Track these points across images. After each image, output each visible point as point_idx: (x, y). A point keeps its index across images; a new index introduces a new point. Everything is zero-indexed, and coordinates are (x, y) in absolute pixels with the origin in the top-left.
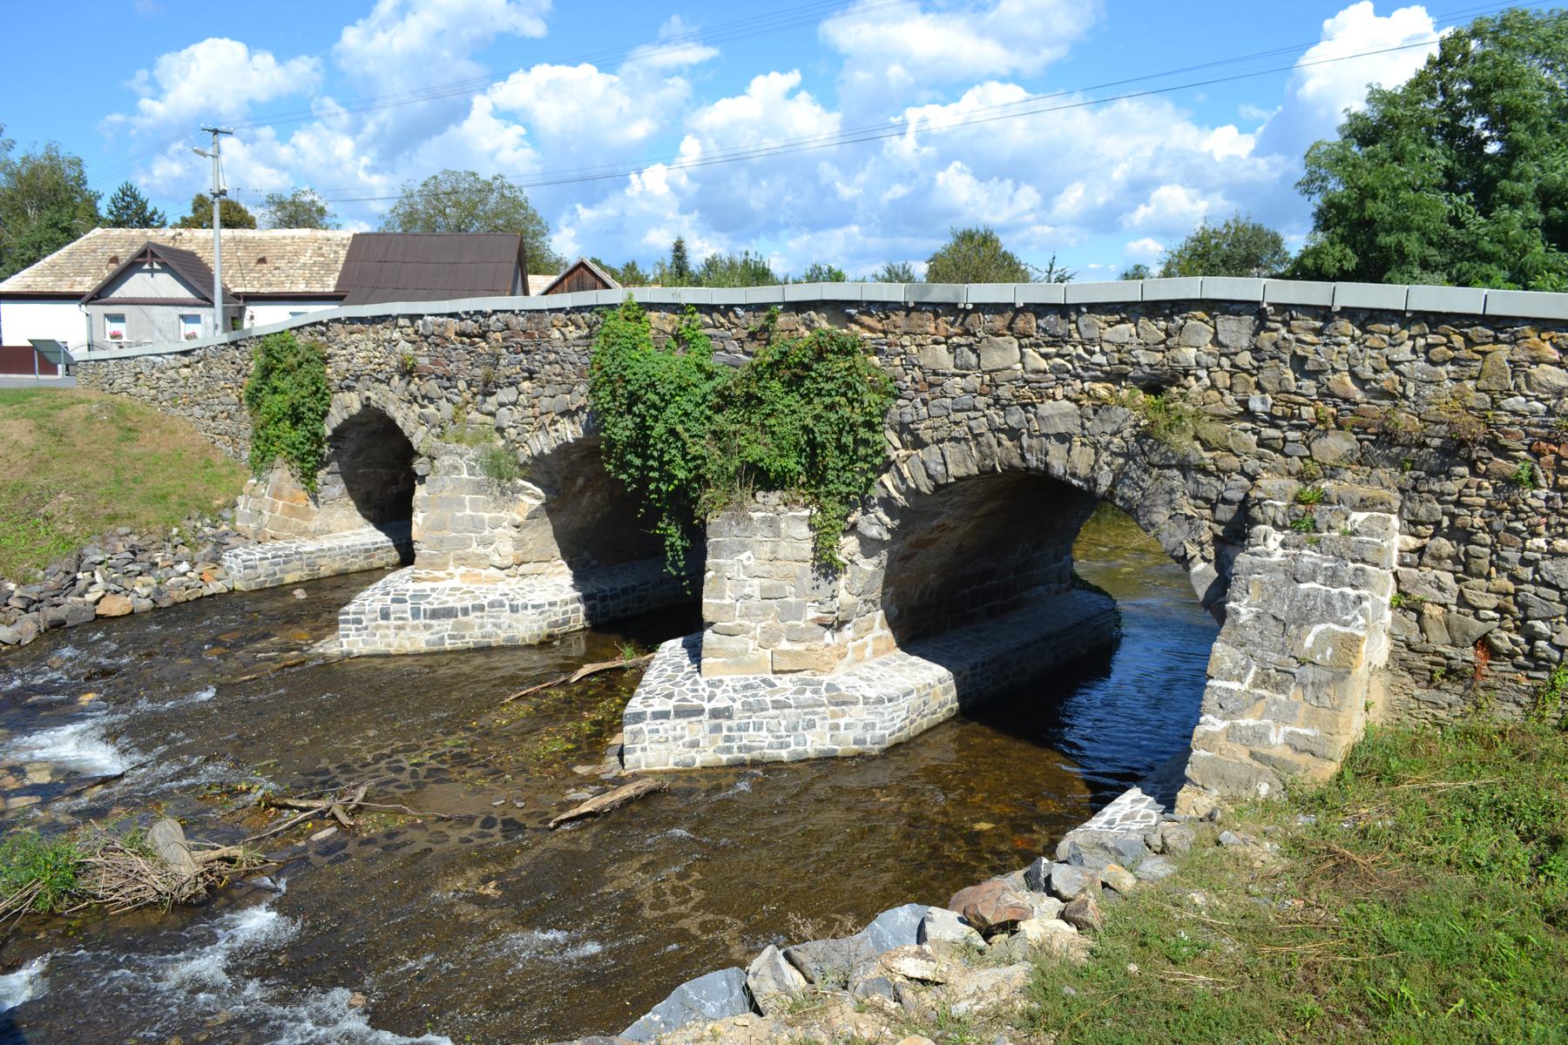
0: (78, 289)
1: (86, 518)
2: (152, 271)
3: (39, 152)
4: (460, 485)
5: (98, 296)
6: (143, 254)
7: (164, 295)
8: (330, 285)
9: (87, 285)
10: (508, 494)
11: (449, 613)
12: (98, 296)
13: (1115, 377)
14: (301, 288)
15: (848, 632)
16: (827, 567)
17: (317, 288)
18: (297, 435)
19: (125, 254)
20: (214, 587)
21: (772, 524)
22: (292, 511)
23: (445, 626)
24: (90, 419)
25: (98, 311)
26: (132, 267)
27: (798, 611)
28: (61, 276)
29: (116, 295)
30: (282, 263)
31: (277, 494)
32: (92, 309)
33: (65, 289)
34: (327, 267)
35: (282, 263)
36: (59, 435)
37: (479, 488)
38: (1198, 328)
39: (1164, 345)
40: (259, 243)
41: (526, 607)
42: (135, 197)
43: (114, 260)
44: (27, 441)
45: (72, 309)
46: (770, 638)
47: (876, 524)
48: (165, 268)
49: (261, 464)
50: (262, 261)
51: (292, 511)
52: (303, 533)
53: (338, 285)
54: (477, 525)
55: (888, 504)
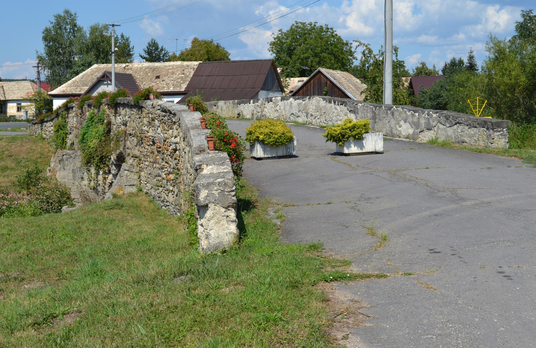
14: (171, 89)
17: (178, 90)
35: (166, 78)
50: (158, 77)
53: (186, 88)
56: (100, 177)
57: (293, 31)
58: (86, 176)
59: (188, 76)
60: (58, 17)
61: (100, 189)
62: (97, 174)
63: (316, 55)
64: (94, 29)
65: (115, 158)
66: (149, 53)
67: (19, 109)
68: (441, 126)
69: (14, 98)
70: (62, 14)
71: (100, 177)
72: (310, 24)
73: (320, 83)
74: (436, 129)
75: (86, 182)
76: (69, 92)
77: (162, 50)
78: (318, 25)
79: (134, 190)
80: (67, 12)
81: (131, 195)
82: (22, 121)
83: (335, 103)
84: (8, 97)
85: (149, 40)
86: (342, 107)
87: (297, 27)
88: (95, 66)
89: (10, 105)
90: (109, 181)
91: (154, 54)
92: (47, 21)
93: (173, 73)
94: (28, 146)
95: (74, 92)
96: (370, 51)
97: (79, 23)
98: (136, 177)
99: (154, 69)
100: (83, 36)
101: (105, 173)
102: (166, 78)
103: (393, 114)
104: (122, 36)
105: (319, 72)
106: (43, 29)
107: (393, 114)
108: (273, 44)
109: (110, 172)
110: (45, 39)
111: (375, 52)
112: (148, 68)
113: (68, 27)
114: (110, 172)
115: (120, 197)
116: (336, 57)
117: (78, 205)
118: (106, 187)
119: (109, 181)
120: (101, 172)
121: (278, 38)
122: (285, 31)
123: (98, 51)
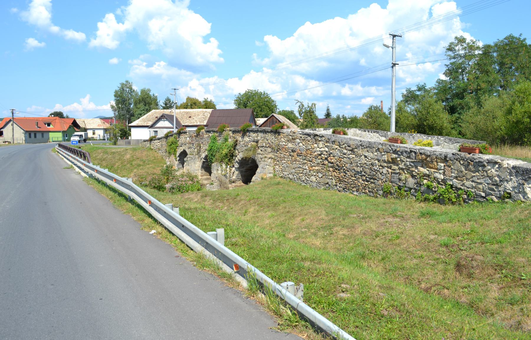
0: (148, 125)
2: (164, 121)
5: (152, 127)
6: (162, 116)
9: (150, 124)
12: (152, 127)
13: (254, 141)
19: (159, 116)
25: (152, 130)
26: (159, 120)
35: (194, 118)
39: (257, 137)
43: (157, 117)
45: (146, 130)
47: (237, 165)
48: (167, 120)
50: (190, 117)
55: (237, 161)
56: (228, 169)
57: (246, 94)
58: (220, 169)
59: (206, 117)
60: (122, 84)
61: (228, 175)
62: (227, 167)
63: (259, 107)
64: (143, 91)
65: (240, 159)
66: (166, 104)
67: (94, 134)
68: (446, 144)
69: (92, 128)
70: (125, 83)
71: (228, 169)
72: (255, 91)
74: (442, 145)
75: (220, 172)
76: (140, 124)
77: (173, 102)
78: (259, 91)
79: (272, 175)
80: (127, 82)
81: (271, 178)
82: (96, 140)
83: (368, 132)
84: (87, 127)
85: (166, 97)
86: (375, 134)
87: (249, 92)
88: (153, 111)
90: (232, 171)
91: (168, 105)
92: (116, 86)
93: (198, 115)
94: (145, 153)
95: (143, 125)
96: (303, 106)
97: (134, 88)
98: (272, 169)
99: (187, 113)
100: (137, 94)
101: (230, 167)
102: (194, 118)
103: (413, 138)
104: (154, 95)
105: (273, 116)
106: (114, 91)
107: (413, 138)
108: (236, 100)
109: (233, 166)
110: (115, 96)
111: (306, 106)
112: (184, 112)
113: (127, 89)
114: (233, 166)
115: (266, 179)
116: (269, 108)
117: (215, 184)
118: (231, 174)
119: (232, 171)
120: (228, 167)
121: (238, 97)
122: (242, 94)
123: (145, 102)
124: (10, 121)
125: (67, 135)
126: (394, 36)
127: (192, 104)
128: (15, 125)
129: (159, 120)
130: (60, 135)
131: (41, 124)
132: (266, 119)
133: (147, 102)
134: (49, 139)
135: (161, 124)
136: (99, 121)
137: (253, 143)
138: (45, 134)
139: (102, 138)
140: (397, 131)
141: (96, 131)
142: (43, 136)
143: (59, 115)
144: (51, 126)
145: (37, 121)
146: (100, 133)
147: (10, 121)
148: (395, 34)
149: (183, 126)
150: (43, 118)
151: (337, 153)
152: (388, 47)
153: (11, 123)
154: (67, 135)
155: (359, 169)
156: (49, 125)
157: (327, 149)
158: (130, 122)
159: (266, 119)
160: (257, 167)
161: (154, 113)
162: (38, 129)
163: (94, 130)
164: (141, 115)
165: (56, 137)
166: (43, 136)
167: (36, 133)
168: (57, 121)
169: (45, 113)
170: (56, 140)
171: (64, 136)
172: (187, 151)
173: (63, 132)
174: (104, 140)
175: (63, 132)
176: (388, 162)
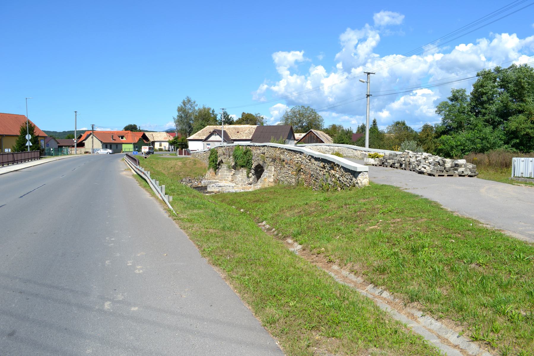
0: (203, 138)
1: (184, 175)
3: (201, 107)
4: (225, 170)
5: (205, 140)
6: (214, 132)
7: (218, 140)
8: (250, 137)
9: (204, 138)
10: (231, 171)
11: (221, 186)
12: (205, 140)
14: (244, 138)
15: (252, 185)
16: (248, 177)
17: (248, 138)
18: (213, 164)
19: (212, 131)
20: (200, 186)
21: (242, 171)
22: (213, 176)
23: (220, 188)
24: (190, 162)
25: (205, 143)
26: (211, 134)
27: (245, 182)
28: (200, 136)
29: (209, 140)
30: (242, 133)
31: (210, 173)
32: (204, 143)
33: (200, 139)
34: (250, 133)
35: (242, 133)
36: (185, 164)
37: (227, 170)
38: (266, 148)
40: (238, 128)
41: (423, 247)
42: (227, 114)
44: (180, 165)
45: (201, 142)
46: (242, 185)
47: (253, 171)
48: (218, 134)
49: (209, 168)
50: (238, 132)
51: (213, 176)
52: (214, 179)
54: (227, 175)
67: (160, 145)
73: (311, 136)
76: (197, 138)
88: (208, 126)
89: (156, 143)
92: (179, 104)
124: (91, 134)
125: (137, 147)
126: (369, 74)
127: (247, 119)
128: (94, 138)
129: (211, 134)
130: (131, 146)
131: (116, 137)
132: (304, 134)
133: (206, 118)
134: (122, 149)
135: (213, 138)
136: (165, 134)
137: (487, 160)
138: (119, 146)
139: (167, 149)
140: (370, 147)
141: (163, 144)
142: (117, 147)
143: (132, 128)
144: (124, 139)
145: (112, 134)
146: (166, 145)
147: (91, 134)
148: (369, 72)
149: (232, 140)
150: (118, 132)
151: (304, 162)
152: (363, 82)
153: (92, 136)
154: (137, 147)
155: (312, 173)
156: (122, 137)
157: (300, 159)
158: (190, 134)
159: (304, 134)
160: (263, 171)
161: (209, 128)
162: (114, 142)
163: (160, 142)
164: (198, 129)
165: (128, 148)
166: (117, 147)
167: (113, 145)
168: (129, 134)
169: (119, 127)
170: (128, 151)
171: (135, 147)
172: (224, 161)
173: (134, 144)
174: (169, 151)
175: (134, 144)
176: (322, 168)
